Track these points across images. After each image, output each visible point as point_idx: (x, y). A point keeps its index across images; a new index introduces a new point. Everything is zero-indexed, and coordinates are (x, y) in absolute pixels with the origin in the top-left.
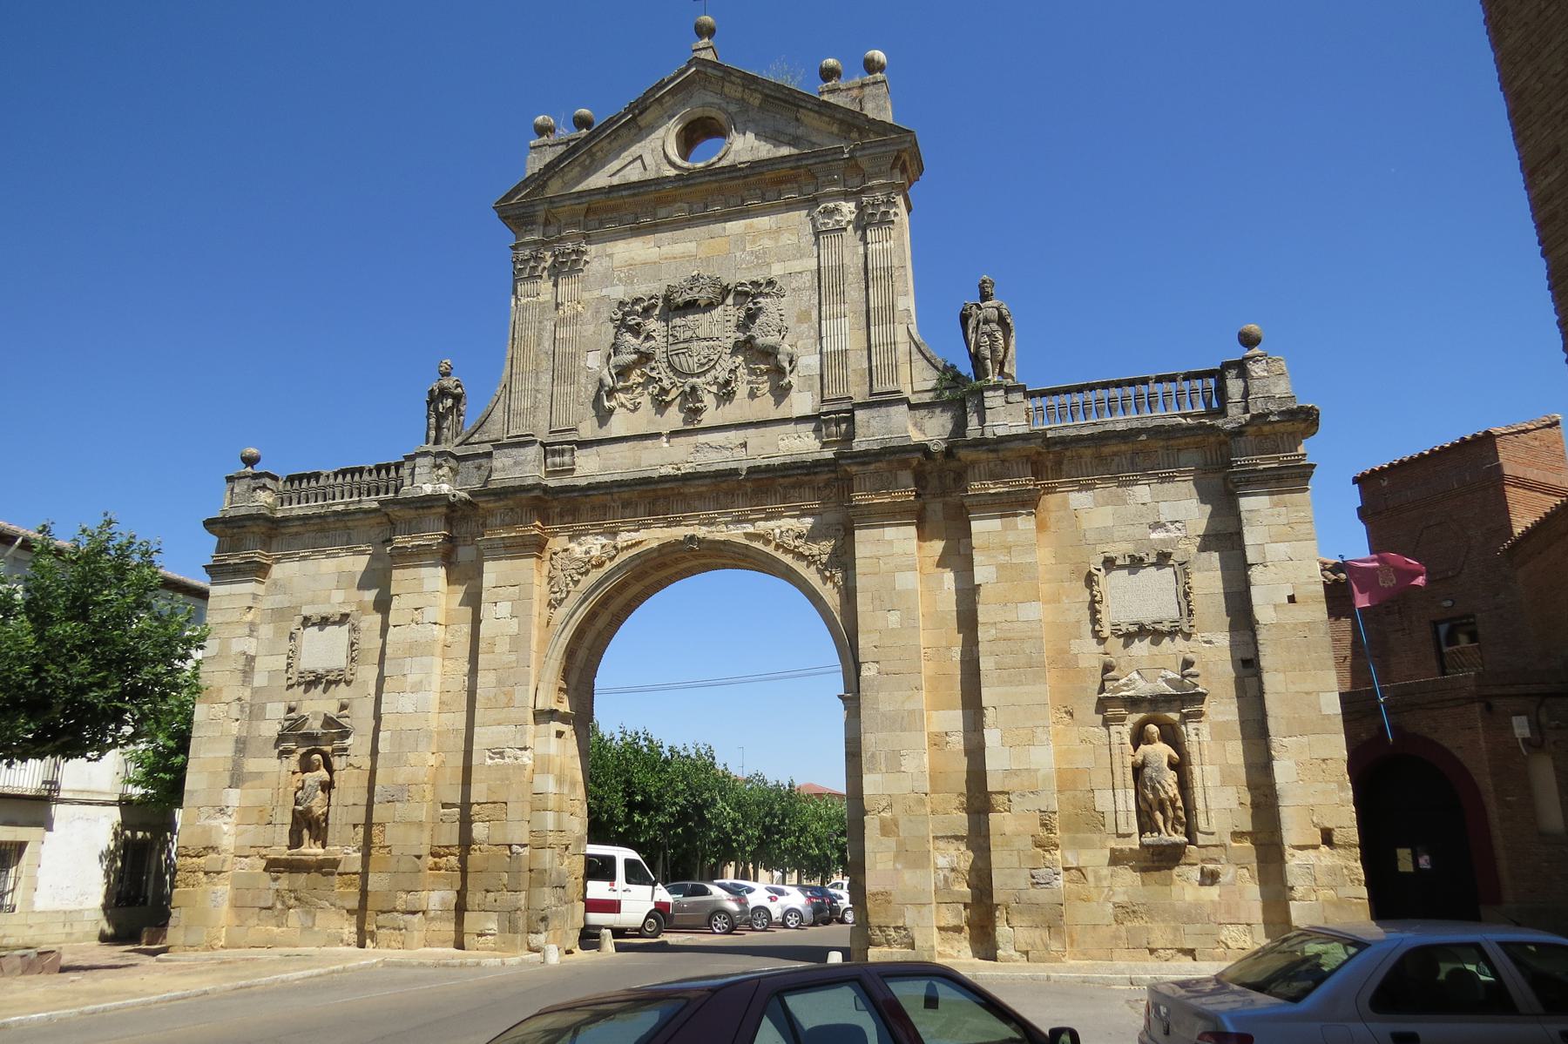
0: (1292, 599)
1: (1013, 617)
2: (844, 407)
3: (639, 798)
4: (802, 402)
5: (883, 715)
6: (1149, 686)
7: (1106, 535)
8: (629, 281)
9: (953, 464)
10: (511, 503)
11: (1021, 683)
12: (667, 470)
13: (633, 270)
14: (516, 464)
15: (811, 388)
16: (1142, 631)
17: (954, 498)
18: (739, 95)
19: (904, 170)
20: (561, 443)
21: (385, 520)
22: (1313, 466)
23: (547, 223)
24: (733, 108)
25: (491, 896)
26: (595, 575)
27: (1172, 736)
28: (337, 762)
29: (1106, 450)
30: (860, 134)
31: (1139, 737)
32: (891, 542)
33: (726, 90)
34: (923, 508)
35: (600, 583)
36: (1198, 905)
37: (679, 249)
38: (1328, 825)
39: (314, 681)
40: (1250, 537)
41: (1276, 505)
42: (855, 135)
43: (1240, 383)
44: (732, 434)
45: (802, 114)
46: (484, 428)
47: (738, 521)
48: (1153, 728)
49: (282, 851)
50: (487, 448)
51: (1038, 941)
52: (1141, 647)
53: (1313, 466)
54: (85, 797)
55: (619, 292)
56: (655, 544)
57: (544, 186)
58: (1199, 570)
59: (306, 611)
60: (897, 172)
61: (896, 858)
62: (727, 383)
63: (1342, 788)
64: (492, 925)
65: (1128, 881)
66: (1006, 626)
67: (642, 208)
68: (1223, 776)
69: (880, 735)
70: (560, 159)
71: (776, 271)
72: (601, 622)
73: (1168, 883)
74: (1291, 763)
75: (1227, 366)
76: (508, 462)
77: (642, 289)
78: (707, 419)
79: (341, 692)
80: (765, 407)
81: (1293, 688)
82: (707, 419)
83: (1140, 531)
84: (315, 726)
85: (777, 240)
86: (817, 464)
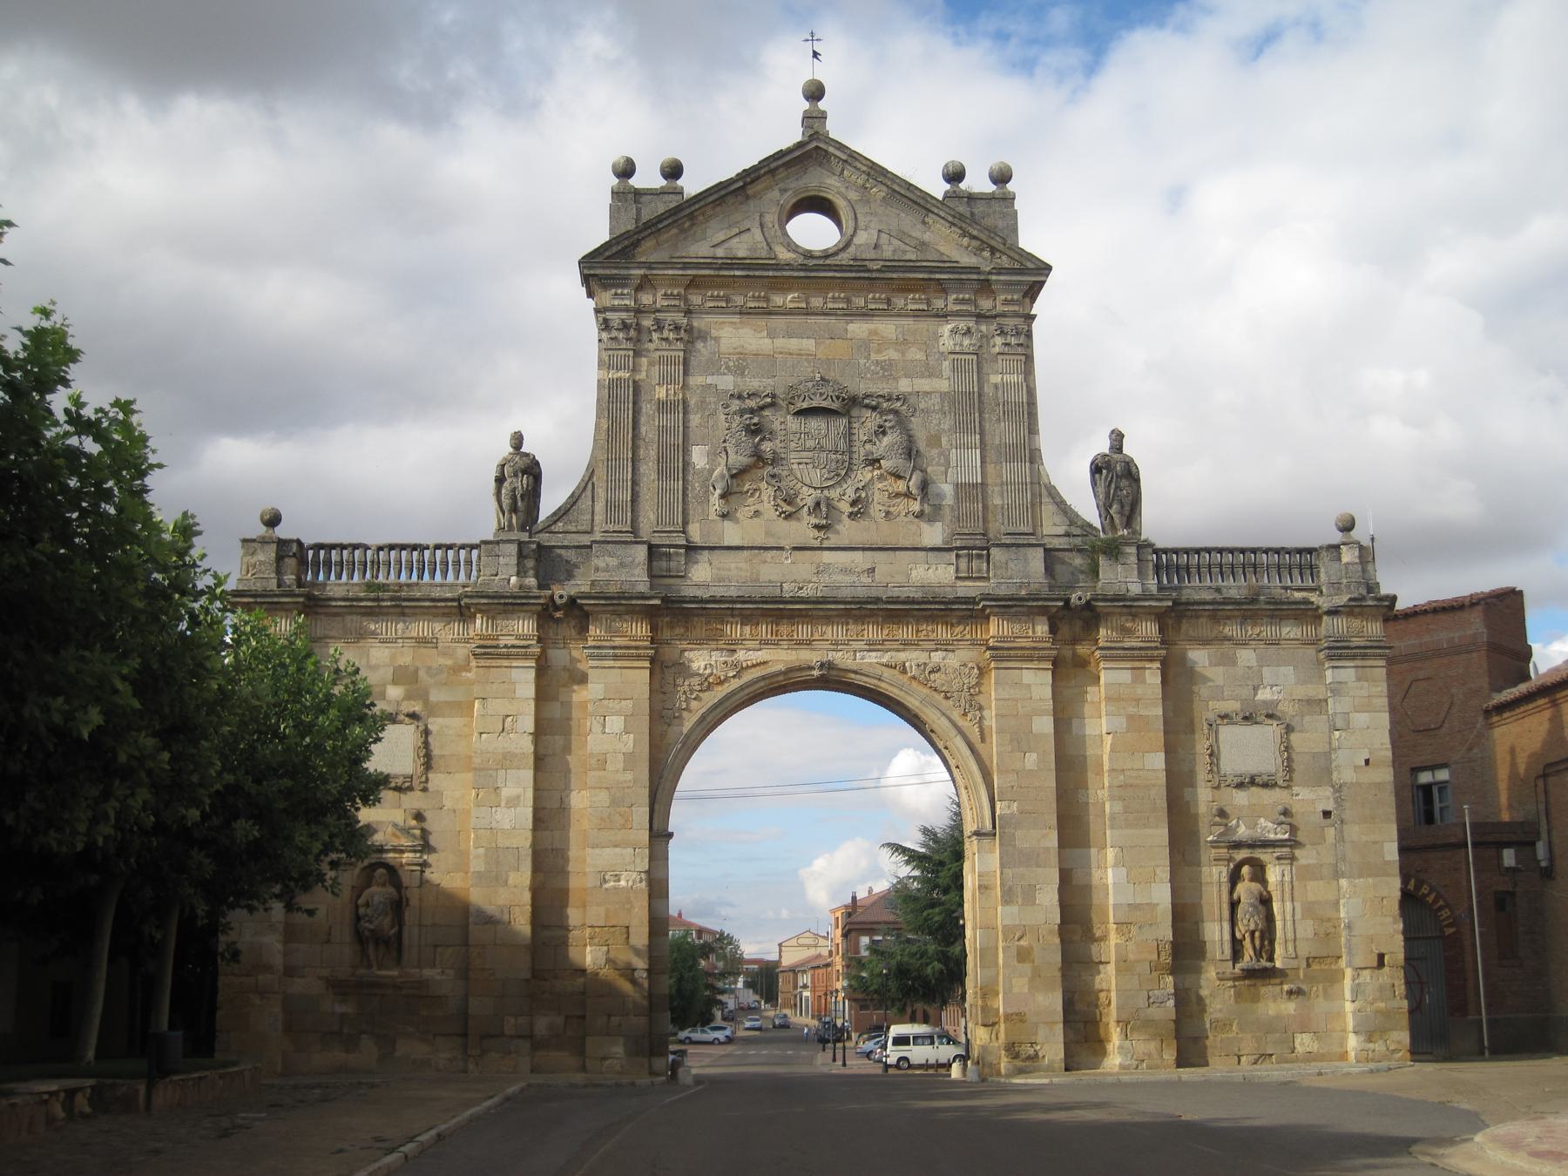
0: (1367, 762)
1: (1138, 765)
3: (73, 483)
4: (933, 534)
8: (740, 371)
11: (1145, 826)
12: (789, 590)
30: (993, 254)
36: (1278, 1017)
37: (794, 344)
41: (1359, 679)
44: (858, 555)
47: (872, 646)
51: (1154, 1052)
55: (727, 382)
56: (781, 667)
61: (1032, 980)
66: (1134, 774)
71: (904, 386)
73: (1256, 999)
76: (613, 562)
77: (754, 384)
79: (413, 801)
81: (1364, 838)
83: (1246, 692)
85: (903, 354)
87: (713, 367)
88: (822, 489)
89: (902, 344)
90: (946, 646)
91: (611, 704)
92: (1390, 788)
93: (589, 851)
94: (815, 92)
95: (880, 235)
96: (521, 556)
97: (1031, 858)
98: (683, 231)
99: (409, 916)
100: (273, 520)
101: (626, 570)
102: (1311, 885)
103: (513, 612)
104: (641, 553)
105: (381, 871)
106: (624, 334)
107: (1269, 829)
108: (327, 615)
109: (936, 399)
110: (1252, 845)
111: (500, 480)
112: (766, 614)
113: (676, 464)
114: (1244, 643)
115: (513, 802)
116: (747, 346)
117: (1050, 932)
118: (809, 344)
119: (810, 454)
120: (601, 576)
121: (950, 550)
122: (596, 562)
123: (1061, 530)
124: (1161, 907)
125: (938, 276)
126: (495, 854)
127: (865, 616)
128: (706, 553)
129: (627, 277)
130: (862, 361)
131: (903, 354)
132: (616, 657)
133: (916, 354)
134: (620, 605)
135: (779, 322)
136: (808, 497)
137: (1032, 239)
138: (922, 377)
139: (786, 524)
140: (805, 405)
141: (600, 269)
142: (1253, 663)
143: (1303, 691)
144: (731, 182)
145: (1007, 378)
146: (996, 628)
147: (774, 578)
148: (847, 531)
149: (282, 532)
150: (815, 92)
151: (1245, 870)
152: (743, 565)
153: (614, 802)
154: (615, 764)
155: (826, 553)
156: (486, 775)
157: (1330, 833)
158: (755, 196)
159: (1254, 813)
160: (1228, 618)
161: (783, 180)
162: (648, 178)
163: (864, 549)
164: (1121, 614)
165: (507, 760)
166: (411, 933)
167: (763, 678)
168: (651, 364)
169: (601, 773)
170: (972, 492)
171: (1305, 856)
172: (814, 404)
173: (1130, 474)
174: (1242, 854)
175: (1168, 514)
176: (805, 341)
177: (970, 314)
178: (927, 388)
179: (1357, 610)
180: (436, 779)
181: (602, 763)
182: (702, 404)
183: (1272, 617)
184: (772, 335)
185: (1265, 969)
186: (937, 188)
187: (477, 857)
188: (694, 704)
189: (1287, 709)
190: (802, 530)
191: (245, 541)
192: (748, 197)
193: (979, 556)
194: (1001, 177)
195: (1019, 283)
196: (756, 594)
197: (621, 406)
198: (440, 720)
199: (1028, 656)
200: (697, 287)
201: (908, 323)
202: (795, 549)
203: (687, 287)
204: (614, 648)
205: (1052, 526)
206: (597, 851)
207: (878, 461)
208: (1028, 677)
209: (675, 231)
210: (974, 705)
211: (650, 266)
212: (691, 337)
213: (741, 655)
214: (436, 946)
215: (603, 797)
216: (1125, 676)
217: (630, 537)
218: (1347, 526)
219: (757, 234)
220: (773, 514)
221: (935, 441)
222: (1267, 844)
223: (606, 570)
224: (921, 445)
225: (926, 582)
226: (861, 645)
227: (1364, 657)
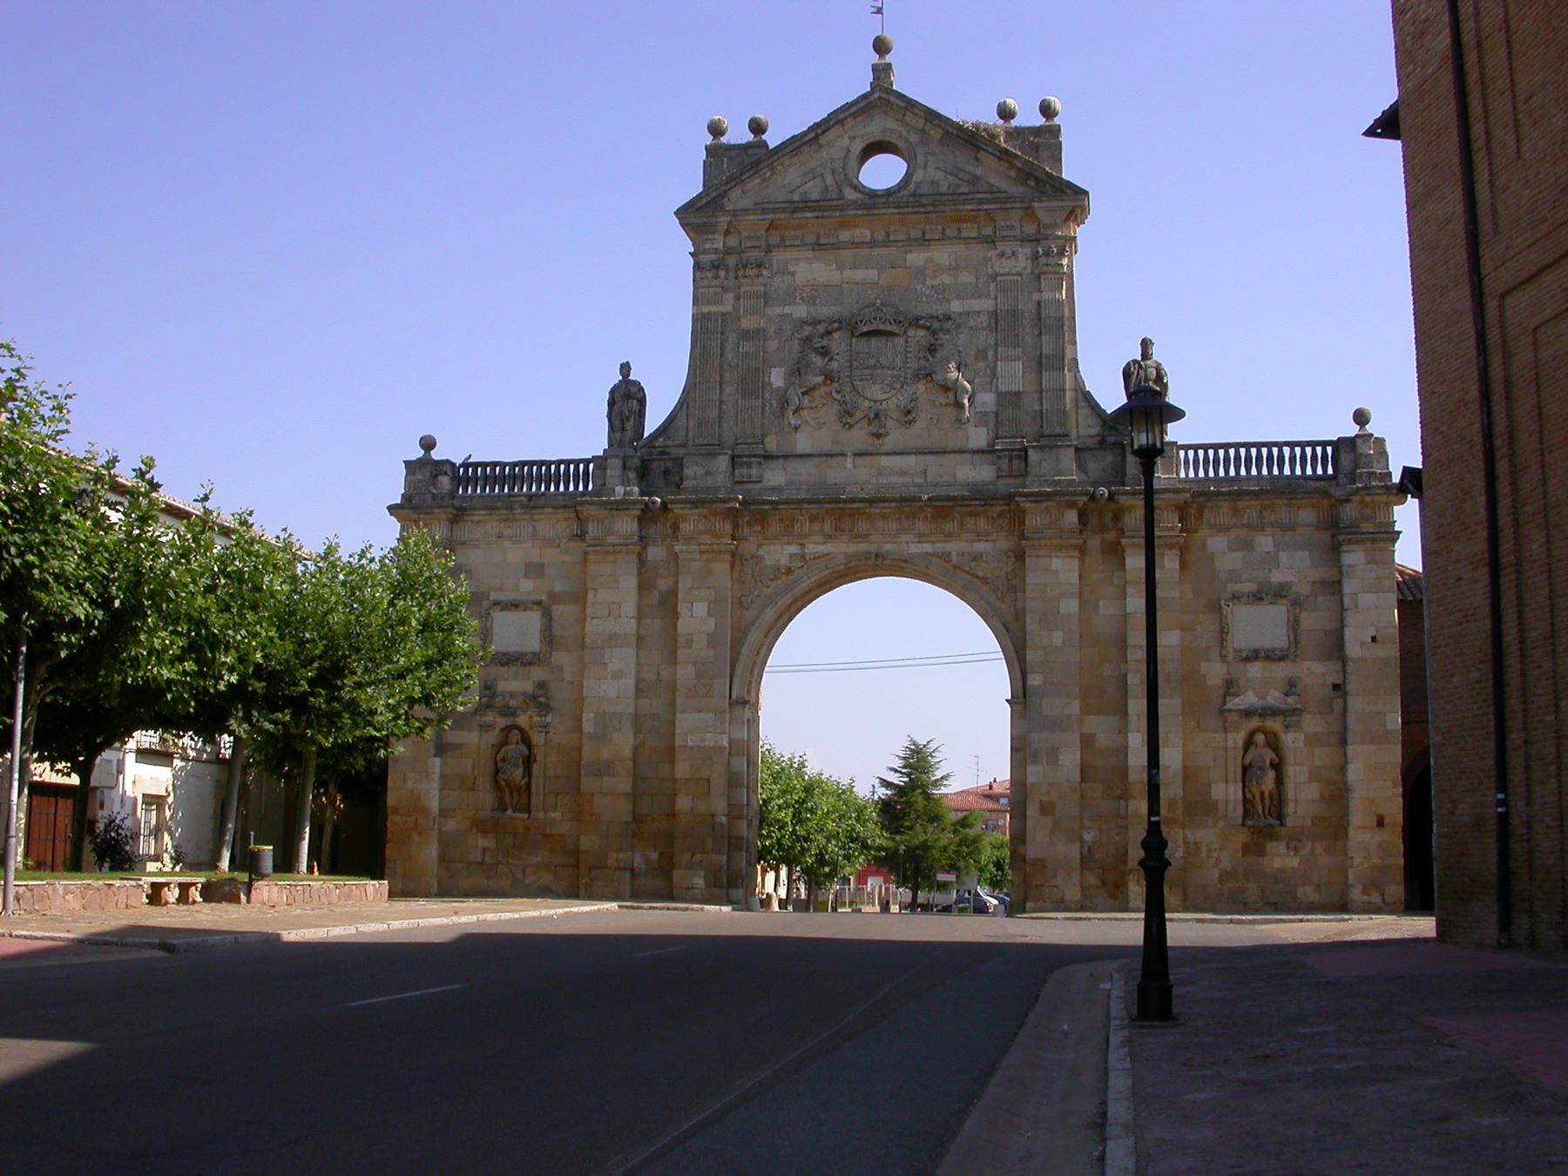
0: (1374, 639)
4: (979, 437)
7: (1234, 576)
8: (812, 301)
9: (1112, 506)
10: (705, 511)
13: (815, 292)
14: (707, 473)
15: (986, 424)
16: (1255, 655)
17: (1111, 536)
18: (920, 125)
21: (573, 515)
23: (727, 233)
24: (913, 138)
29: (1240, 504)
32: (1057, 572)
33: (907, 118)
37: (860, 275)
38: (1381, 811)
40: (1348, 587)
41: (1368, 562)
42: (1032, 183)
43: (1351, 456)
44: (911, 459)
45: (981, 155)
47: (921, 538)
52: (1255, 670)
54: (1513, 701)
55: (801, 311)
57: (724, 195)
63: (1395, 786)
64: (699, 881)
71: (956, 306)
76: (700, 471)
77: (824, 311)
78: (890, 442)
79: (538, 673)
85: (956, 277)
87: (789, 297)
100: (428, 444)
107: (1274, 697)
109: (984, 318)
113: (752, 382)
115: (618, 675)
118: (873, 274)
128: (781, 461)
131: (956, 277)
133: (966, 278)
135: (847, 255)
138: (972, 297)
140: (865, 329)
148: (896, 436)
149: (436, 455)
150: (881, 46)
174: (1255, 722)
184: (840, 268)
190: (858, 437)
192: (821, 146)
195: (1060, 208)
197: (706, 333)
200: (776, 229)
218: (1361, 418)
220: (839, 426)
222: (1274, 712)
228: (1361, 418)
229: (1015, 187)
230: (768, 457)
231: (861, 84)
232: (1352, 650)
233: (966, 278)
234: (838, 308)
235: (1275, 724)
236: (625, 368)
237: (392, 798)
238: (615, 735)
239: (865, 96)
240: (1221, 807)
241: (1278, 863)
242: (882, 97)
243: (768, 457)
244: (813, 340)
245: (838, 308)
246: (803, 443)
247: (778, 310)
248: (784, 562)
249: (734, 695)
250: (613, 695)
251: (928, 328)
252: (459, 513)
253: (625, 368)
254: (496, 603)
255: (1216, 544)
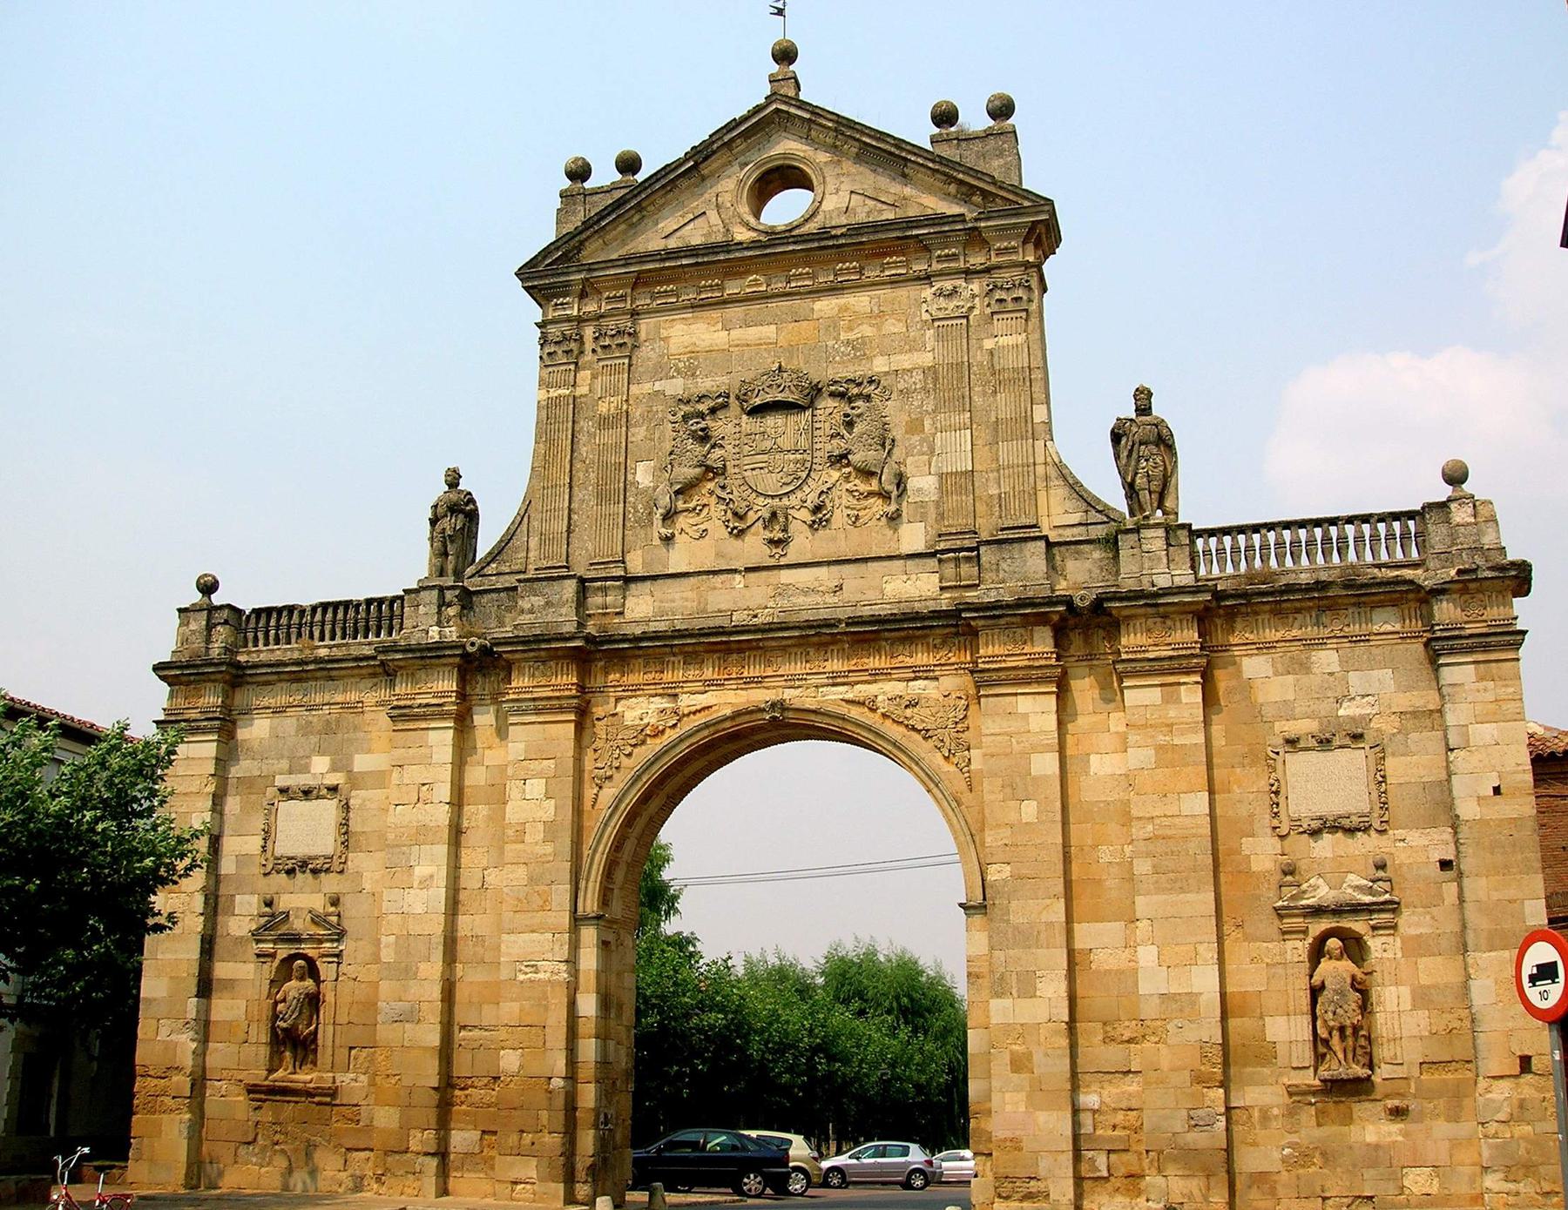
0: (1497, 791)
2: (967, 544)
4: (913, 537)
5: (1016, 928)
6: (1333, 893)
12: (739, 618)
19: (1038, 245)
20: (606, 579)
22: (1524, 633)
25: (528, 1138)
26: (654, 746)
27: (1354, 947)
28: (326, 970)
31: (1317, 952)
32: (1025, 716)
33: (813, 133)
34: (1065, 673)
35: (657, 757)
37: (753, 333)
39: (298, 867)
41: (1481, 679)
42: (977, 199)
44: (822, 572)
46: (504, 556)
47: (835, 680)
48: (1333, 943)
49: (258, 1075)
50: (510, 581)
51: (1196, 1192)
52: (1327, 844)
53: (1524, 633)
55: (675, 387)
56: (728, 712)
57: (580, 247)
58: (1393, 754)
59: (281, 781)
60: (1030, 247)
62: (817, 509)
65: (1309, 1130)
66: (1166, 822)
67: (709, 271)
68: (1414, 1000)
69: (1011, 952)
70: (601, 215)
71: (880, 365)
72: (670, 787)
73: (1348, 1119)
74: (1490, 982)
75: (1429, 507)
76: (538, 601)
77: (706, 384)
78: (793, 554)
79: (331, 883)
80: (877, 539)
81: (1495, 896)
82: (793, 554)
83: (1325, 707)
84: (299, 924)
85: (879, 329)
86: (937, 614)
87: (661, 371)
88: (780, 497)
89: (877, 316)
90: (919, 674)
91: (534, 765)
92: (216, 957)
93: (505, 937)
94: (785, 55)
95: (840, 196)
96: (443, 604)
97: (1027, 937)
98: (632, 226)
99: (325, 1013)
100: (208, 587)
101: (554, 610)
102: (1423, 962)
103: (432, 666)
104: (570, 587)
105: (300, 962)
106: (559, 347)
107: (1353, 887)
108: (258, 684)
110: (1338, 911)
111: (433, 522)
112: (713, 649)
113: (615, 487)
114: (1321, 643)
115: (426, 882)
116: (697, 343)
117: (1056, 1032)
118: (769, 331)
119: (765, 457)
120: (525, 619)
121: (933, 555)
122: (524, 604)
123: (1076, 518)
124: (1203, 999)
125: (915, 232)
126: (405, 940)
127: (826, 644)
129: (567, 284)
130: (830, 343)
131: (879, 329)
132: (538, 711)
134: (541, 648)
135: (735, 312)
136: (762, 507)
137: (1037, 175)
139: (737, 543)
140: (758, 401)
141: (543, 277)
142: (1335, 668)
143: (1405, 701)
144: (679, 163)
145: (1003, 341)
146: (993, 649)
147: (723, 607)
148: (803, 544)
149: (217, 599)
150: (785, 55)
151: (1333, 943)
152: (690, 594)
153: (532, 880)
154: (535, 834)
155: (784, 572)
156: (397, 852)
157: (1451, 889)
158: (712, 174)
159: (1340, 868)
160: (1298, 611)
161: (743, 153)
162: (604, 175)
163: (829, 563)
164: (1146, 616)
165: (421, 835)
166: (326, 1036)
167: (706, 726)
168: (594, 377)
169: (521, 846)
170: (958, 482)
171: (1411, 922)
172: (769, 399)
173: (1164, 441)
174: (1318, 926)
175: (1211, 490)
176: (765, 329)
177: (958, 272)
178: (907, 366)
179: (1472, 586)
180: (356, 860)
181: (521, 833)
182: (649, 415)
183: (1358, 605)
185: (1357, 1080)
186: (920, 132)
187: (387, 946)
188: (625, 761)
189: (1384, 725)
190: (754, 547)
191: (180, 610)
192: (703, 179)
193: (968, 559)
194: (1002, 109)
195: (1014, 226)
196: (698, 624)
197: (560, 424)
198: (362, 793)
199: (1023, 678)
200: (646, 284)
201: (885, 293)
202: (748, 570)
203: (634, 287)
204: (534, 699)
205: (1057, 514)
206: (512, 937)
207: (844, 456)
208: (1024, 704)
209: (623, 227)
210: (957, 749)
211: (590, 268)
212: (628, 342)
213: (686, 702)
214: (351, 1048)
215: (521, 873)
216: (1155, 695)
217: (564, 572)
218: (1455, 476)
219: (713, 216)
220: (725, 533)
221: (915, 426)
222: (1356, 909)
223: (531, 612)
224: (897, 433)
225: (904, 597)
226: (822, 679)
227: (1486, 648)
228: (1455, 476)
229: (975, 215)
230: (628, 580)
231: (758, 92)
232: (1467, 809)
233: (893, 326)
234: (725, 379)
235: (1358, 925)
236: (453, 479)
237: (142, 1055)
238: (422, 966)
239: (758, 109)
240: (1281, 1050)
241: (1371, 1137)
242: (782, 111)
243: (628, 580)
244: (698, 418)
245: (725, 379)
246: (677, 560)
247: (647, 387)
248: (652, 719)
249: (580, 909)
250: (419, 909)
251: (842, 395)
252: (236, 677)
253: (453, 479)
254: (283, 791)
255: (1254, 666)
